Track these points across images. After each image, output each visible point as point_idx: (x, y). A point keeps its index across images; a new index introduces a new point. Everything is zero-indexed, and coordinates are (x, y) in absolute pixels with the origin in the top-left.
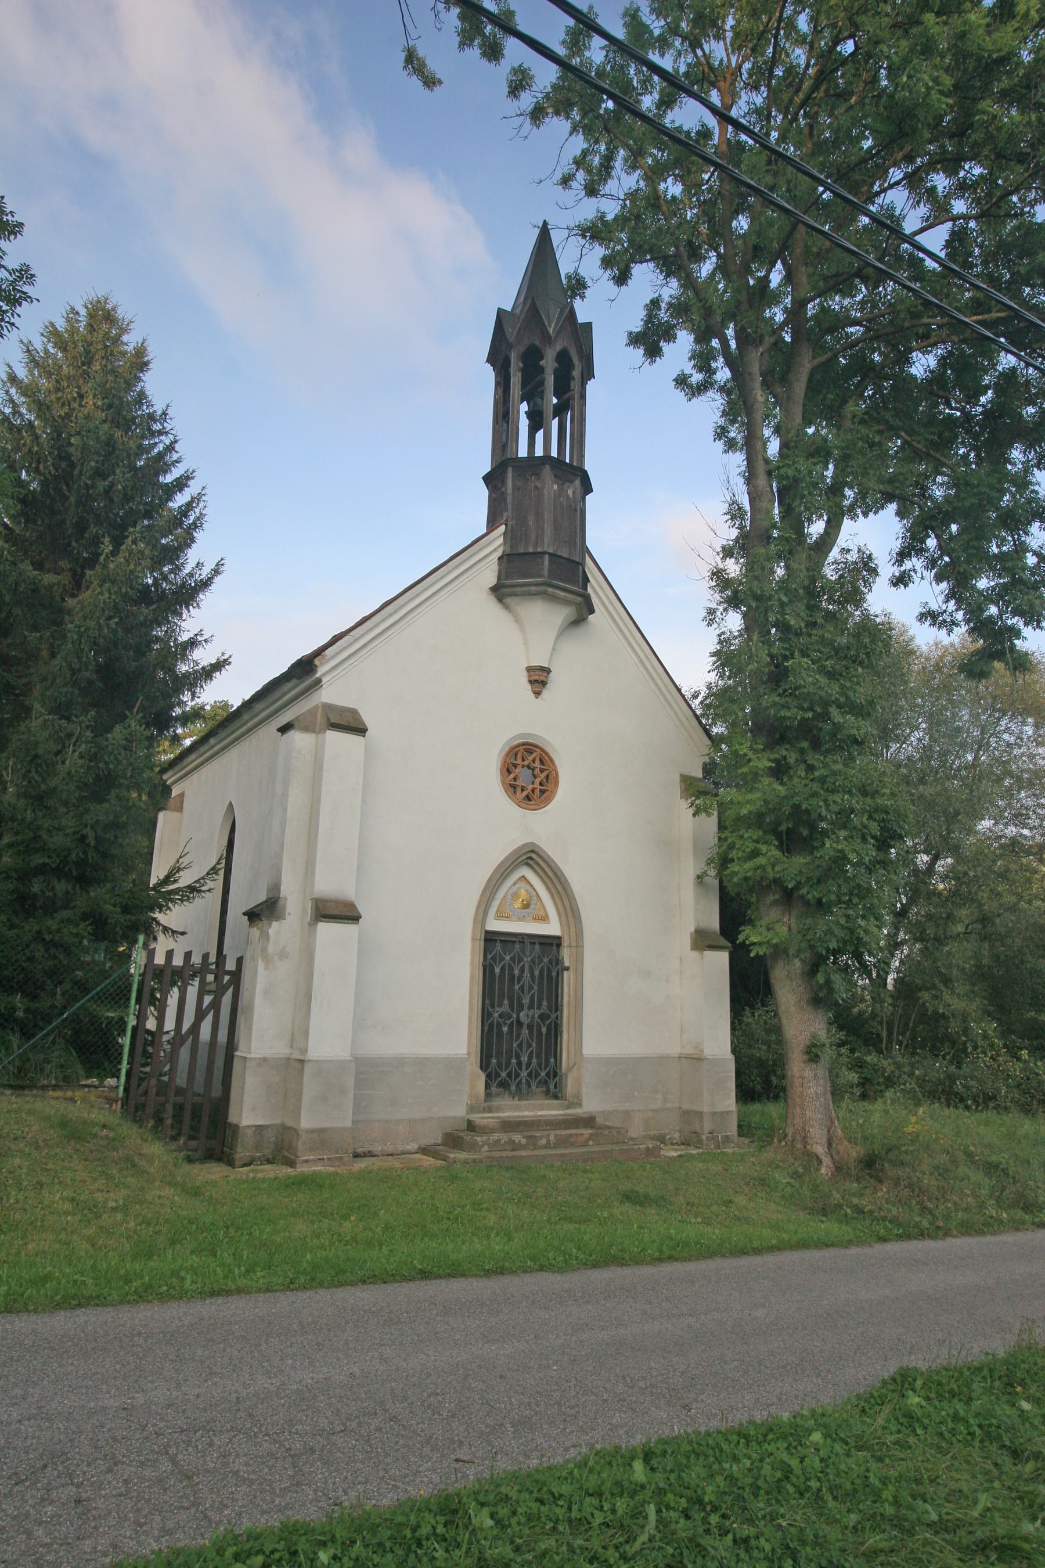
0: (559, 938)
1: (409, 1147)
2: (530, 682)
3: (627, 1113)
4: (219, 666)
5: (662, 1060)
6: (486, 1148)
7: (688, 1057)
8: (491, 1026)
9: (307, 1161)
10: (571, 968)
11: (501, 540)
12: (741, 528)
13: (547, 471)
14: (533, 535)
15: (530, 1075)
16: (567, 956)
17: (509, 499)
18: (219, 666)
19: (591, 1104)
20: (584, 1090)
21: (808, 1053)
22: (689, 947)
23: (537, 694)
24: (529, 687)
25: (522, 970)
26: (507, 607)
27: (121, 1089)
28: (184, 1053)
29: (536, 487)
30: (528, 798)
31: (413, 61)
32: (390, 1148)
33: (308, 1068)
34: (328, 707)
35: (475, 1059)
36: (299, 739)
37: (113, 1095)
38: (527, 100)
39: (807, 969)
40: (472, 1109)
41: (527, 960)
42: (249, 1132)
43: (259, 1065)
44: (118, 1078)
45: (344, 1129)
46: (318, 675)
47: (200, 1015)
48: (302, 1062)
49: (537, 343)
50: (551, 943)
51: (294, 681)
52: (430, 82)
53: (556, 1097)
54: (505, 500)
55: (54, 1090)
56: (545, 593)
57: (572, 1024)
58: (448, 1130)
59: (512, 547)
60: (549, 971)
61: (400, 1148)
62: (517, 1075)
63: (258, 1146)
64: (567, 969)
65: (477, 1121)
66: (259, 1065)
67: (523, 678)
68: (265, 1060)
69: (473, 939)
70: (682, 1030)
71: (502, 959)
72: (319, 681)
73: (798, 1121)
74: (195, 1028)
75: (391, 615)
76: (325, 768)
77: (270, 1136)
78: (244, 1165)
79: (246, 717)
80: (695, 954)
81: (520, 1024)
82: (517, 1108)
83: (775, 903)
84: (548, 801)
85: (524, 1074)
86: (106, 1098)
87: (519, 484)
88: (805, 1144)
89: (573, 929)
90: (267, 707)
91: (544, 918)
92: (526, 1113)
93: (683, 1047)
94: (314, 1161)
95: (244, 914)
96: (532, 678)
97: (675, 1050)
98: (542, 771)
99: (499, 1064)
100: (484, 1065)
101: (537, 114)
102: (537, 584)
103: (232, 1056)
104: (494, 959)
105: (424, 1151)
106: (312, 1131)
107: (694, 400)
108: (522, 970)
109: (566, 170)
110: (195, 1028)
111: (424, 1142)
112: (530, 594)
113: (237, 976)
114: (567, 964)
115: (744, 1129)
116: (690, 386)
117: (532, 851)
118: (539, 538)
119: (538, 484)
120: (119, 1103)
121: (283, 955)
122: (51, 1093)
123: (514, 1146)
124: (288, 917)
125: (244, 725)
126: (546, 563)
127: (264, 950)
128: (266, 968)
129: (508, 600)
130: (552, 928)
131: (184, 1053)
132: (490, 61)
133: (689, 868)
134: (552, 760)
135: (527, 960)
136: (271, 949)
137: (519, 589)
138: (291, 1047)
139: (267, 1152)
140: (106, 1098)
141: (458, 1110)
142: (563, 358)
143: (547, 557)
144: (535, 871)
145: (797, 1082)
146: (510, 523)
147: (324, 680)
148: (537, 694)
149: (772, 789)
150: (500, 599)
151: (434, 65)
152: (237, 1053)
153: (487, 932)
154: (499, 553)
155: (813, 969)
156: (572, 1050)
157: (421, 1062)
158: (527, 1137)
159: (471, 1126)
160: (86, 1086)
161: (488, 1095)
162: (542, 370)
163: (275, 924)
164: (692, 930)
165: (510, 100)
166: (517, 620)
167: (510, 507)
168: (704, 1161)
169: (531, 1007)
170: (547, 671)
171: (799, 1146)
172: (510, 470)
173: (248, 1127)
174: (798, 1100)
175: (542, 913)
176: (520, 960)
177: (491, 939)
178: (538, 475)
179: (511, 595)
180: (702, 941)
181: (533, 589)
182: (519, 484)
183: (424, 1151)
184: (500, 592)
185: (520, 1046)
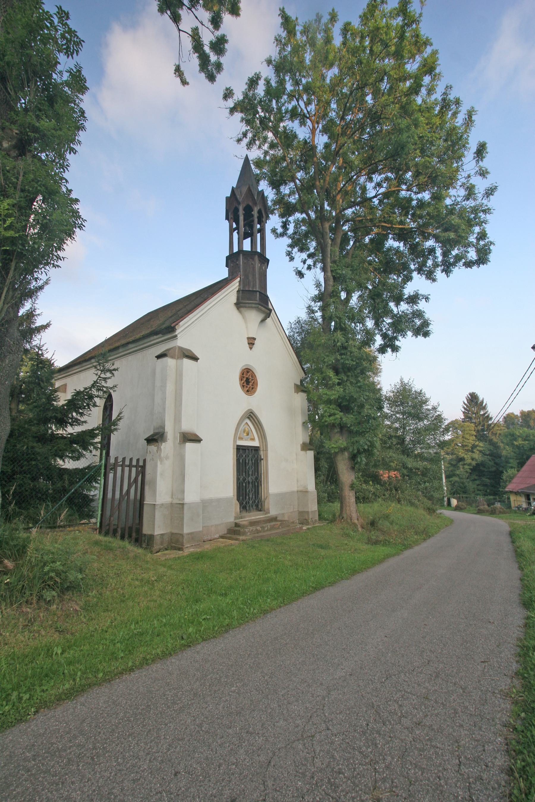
0: (258, 447)
1: (216, 536)
2: (249, 343)
3: (283, 514)
4: (47, 326)
5: (293, 492)
6: (249, 533)
7: (301, 491)
8: (240, 483)
9: (187, 547)
10: (264, 459)
11: (238, 284)
12: (320, 290)
13: (256, 257)
14: (252, 284)
15: (252, 502)
16: (262, 453)
17: (241, 267)
18: (47, 326)
19: (273, 512)
20: (270, 507)
21: (351, 487)
22: (300, 449)
23: (251, 348)
24: (248, 345)
25: (249, 461)
26: (240, 312)
27: (98, 524)
28: (124, 505)
29: (252, 264)
30: (248, 391)
31: (178, 70)
32: (209, 538)
33: (186, 507)
34: (180, 348)
35: (236, 497)
36: (170, 362)
37: (95, 527)
38: (231, 103)
39: (351, 456)
40: (236, 518)
41: (250, 456)
42: (158, 537)
43: (161, 507)
44: (97, 519)
45: (200, 532)
46: (177, 333)
47: (130, 486)
48: (183, 504)
49: (251, 204)
50: (256, 449)
51: (160, 335)
52: (184, 82)
53: (261, 511)
54: (239, 267)
55: (69, 527)
56: (258, 308)
57: (265, 480)
58: (229, 528)
59: (244, 287)
60: (245, 460)
61: (213, 537)
62: (249, 503)
63: (162, 543)
64: (262, 459)
65: (241, 523)
66: (161, 507)
67: (246, 342)
68: (162, 504)
69: (234, 448)
70: (297, 481)
71: (242, 456)
72: (176, 336)
73: (348, 512)
74: (128, 491)
75: (202, 310)
76: (184, 374)
77: (166, 538)
78: (157, 553)
79: (121, 350)
80: (303, 452)
81: (249, 482)
82: (250, 516)
83: (337, 432)
84: (254, 392)
85: (251, 502)
86: (93, 529)
87: (245, 261)
88: (351, 520)
89: (264, 444)
90: (136, 347)
91: (253, 439)
92: (253, 518)
93: (298, 487)
94: (190, 547)
95: (145, 440)
96: (250, 342)
97: (295, 489)
98: (252, 380)
99: (243, 499)
100: (238, 499)
101: (232, 111)
102: (256, 304)
103: (143, 504)
104: (240, 456)
105: (222, 537)
106: (188, 534)
107: (278, 239)
108: (249, 461)
109: (239, 136)
110: (128, 491)
111: (221, 533)
112: (252, 307)
113: (144, 467)
114: (262, 458)
115: (321, 518)
116: (277, 233)
117: (251, 413)
118: (254, 285)
119: (253, 262)
120: (98, 530)
121: (167, 458)
122: (68, 529)
123: (258, 532)
124: (168, 441)
125: (119, 353)
126: (258, 296)
127: (160, 455)
128: (161, 464)
129: (242, 309)
130: (256, 443)
131: (124, 505)
132: (209, 80)
133: (300, 419)
134: (255, 376)
135: (250, 456)
136: (162, 455)
137: (247, 305)
138: (172, 498)
139: (165, 545)
140: (93, 529)
141: (231, 519)
142: (260, 212)
143: (258, 293)
144: (251, 421)
145: (347, 497)
146: (242, 277)
147: (178, 336)
148: (251, 348)
149: (340, 390)
150: (238, 308)
151: (187, 77)
152: (145, 502)
153: (237, 446)
154: (237, 289)
155: (353, 457)
156: (266, 491)
157: (219, 500)
158: (261, 527)
159: (237, 525)
160: (83, 524)
161: (240, 512)
162: (253, 216)
163: (163, 444)
164: (301, 443)
165: (457, 96)
166: (244, 317)
167: (242, 271)
168: (324, 529)
169: (252, 475)
170: (254, 339)
171: (349, 521)
172: (241, 255)
173: (158, 535)
174: (348, 504)
175: (252, 437)
176: (248, 456)
177: (240, 449)
178: (253, 259)
179: (243, 307)
180: (305, 447)
181: (253, 305)
182: (245, 261)
183: (222, 537)
184: (239, 305)
185: (252, 490)
